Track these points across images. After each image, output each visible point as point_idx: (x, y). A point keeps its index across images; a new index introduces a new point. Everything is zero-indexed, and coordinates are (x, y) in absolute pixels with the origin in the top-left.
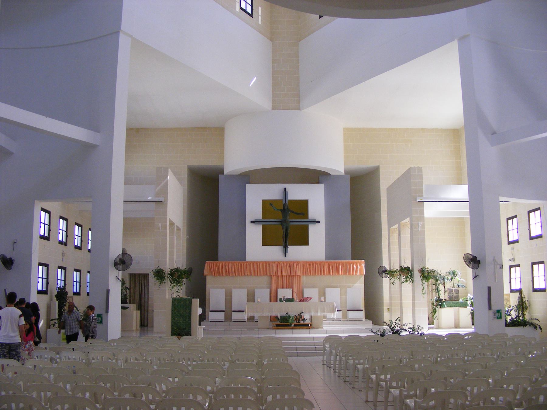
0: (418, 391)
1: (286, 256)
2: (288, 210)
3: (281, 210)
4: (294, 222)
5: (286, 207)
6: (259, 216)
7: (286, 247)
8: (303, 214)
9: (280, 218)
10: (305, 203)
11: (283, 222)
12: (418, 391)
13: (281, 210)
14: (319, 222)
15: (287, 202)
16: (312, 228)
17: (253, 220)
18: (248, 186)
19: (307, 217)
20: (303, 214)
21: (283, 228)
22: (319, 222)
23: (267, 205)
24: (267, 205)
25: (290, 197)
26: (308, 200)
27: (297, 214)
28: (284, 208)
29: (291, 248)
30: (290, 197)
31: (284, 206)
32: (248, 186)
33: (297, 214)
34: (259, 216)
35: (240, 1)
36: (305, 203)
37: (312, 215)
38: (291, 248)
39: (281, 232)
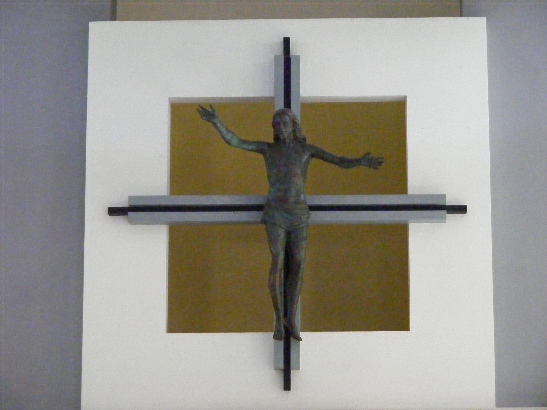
0: (304, 160)
1: (287, 386)
2: (301, 142)
3: (261, 148)
4: (332, 206)
5: (287, 132)
6: (155, 183)
7: (287, 337)
8: (374, 163)
9: (261, 192)
10: (388, 118)
11: (276, 211)
12: (304, 160)
13: (261, 148)
14: (462, 209)
15: (295, 108)
16: (424, 241)
17: (279, 379)
18: (98, 31)
19: (401, 185)
20: (374, 163)
21: (272, 240)
22: (462, 209)
23: (197, 124)
24: (197, 124)
25: (313, 86)
26: (405, 98)
27: (344, 163)
28: (277, 138)
29: (313, 345)
30: (313, 86)
31: (276, 125)
32: (98, 31)
33: (344, 163)
34: (155, 183)
35: (461, 2)
36: (388, 118)
37: (424, 173)
38: (313, 345)
39: (261, 258)
